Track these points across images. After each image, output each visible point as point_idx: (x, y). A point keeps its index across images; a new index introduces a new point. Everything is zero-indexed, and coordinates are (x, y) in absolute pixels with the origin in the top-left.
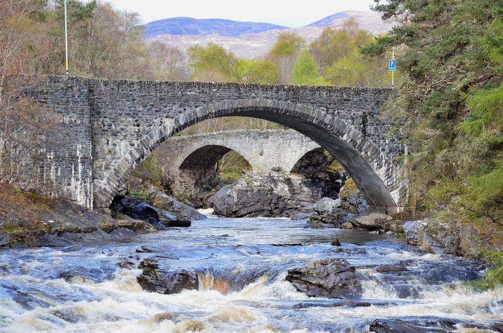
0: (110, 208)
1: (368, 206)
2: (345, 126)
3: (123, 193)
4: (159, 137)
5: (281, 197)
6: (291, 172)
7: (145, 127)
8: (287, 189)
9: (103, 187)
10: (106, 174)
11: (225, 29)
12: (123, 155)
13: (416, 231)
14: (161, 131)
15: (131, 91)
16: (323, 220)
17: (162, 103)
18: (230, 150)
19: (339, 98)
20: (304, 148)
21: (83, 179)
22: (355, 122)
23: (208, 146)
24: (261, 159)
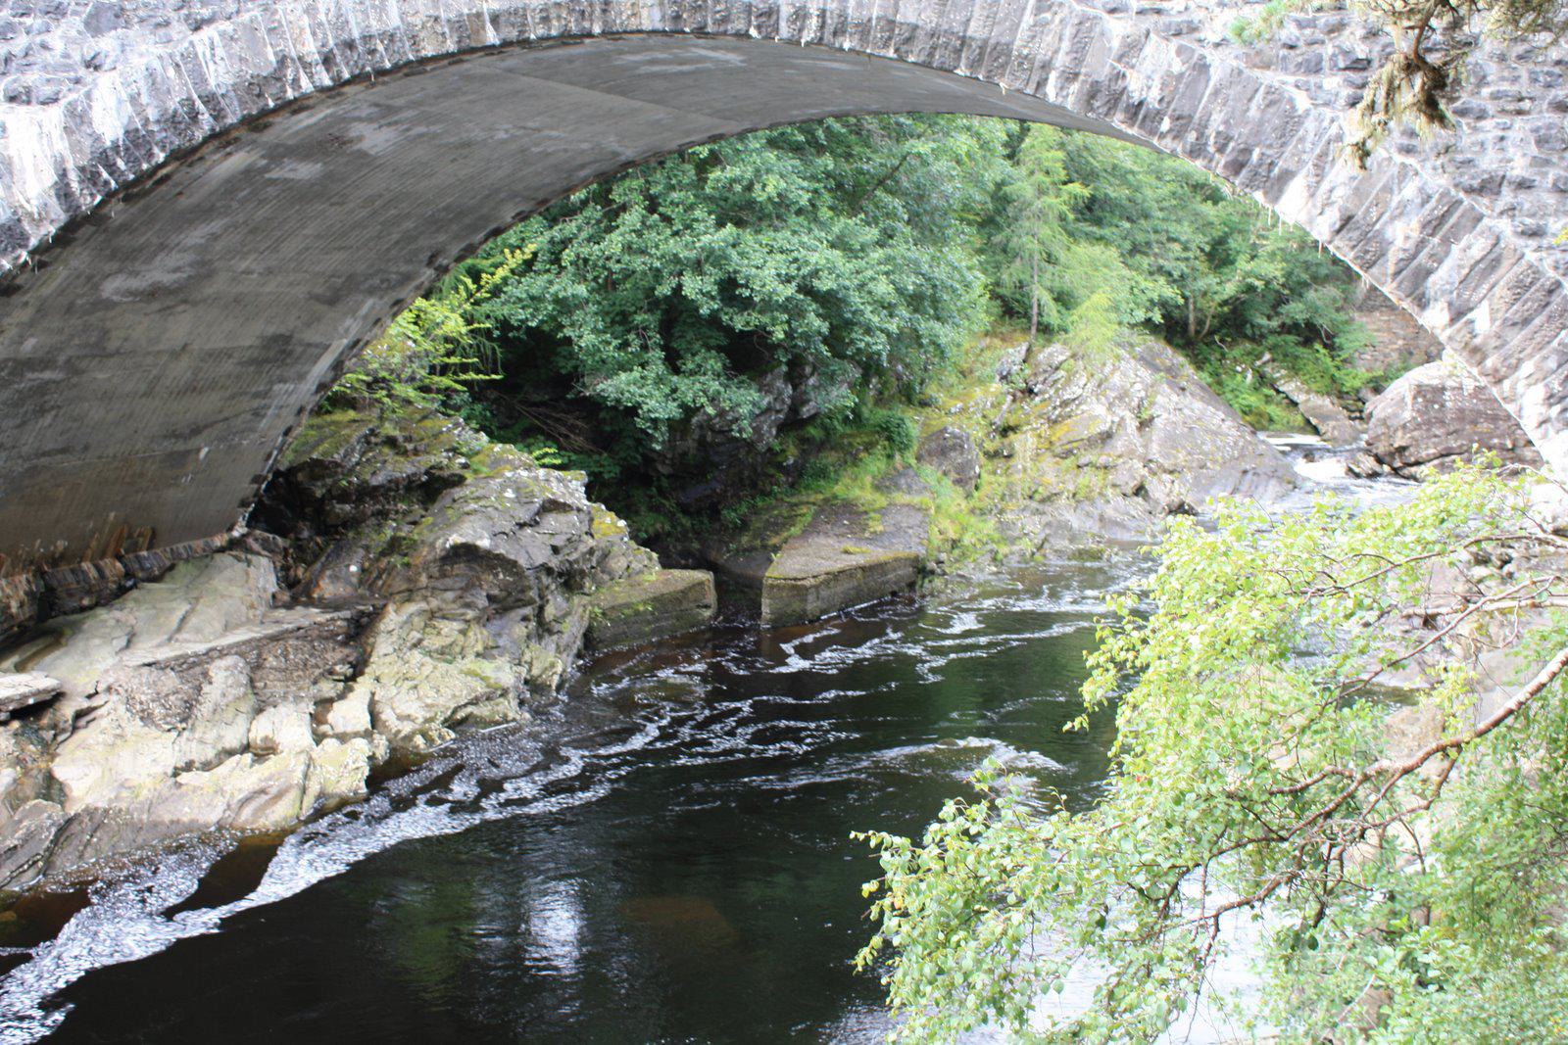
2: (1291, 123)
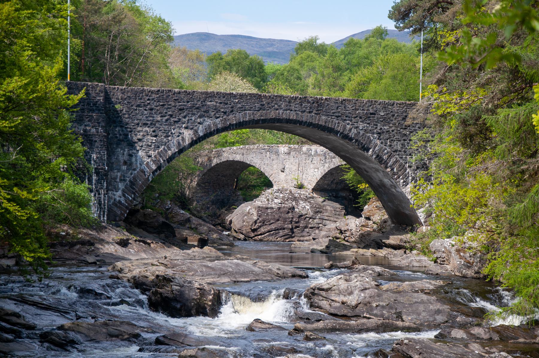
0: (124, 221)
1: (393, 225)
3: (139, 207)
4: (177, 148)
5: (302, 216)
6: (313, 189)
7: (162, 137)
8: (309, 207)
9: (118, 199)
10: (121, 186)
11: (247, 46)
12: (139, 166)
13: (443, 250)
14: (179, 143)
15: (149, 100)
16: (346, 239)
17: (180, 114)
18: (250, 165)
19: (365, 112)
20: (327, 165)
21: (97, 191)
22: (382, 137)
23: (227, 161)
24: (282, 175)
